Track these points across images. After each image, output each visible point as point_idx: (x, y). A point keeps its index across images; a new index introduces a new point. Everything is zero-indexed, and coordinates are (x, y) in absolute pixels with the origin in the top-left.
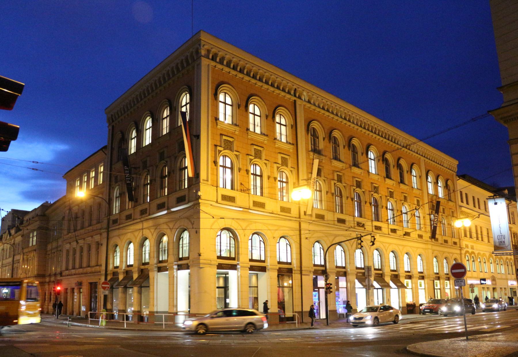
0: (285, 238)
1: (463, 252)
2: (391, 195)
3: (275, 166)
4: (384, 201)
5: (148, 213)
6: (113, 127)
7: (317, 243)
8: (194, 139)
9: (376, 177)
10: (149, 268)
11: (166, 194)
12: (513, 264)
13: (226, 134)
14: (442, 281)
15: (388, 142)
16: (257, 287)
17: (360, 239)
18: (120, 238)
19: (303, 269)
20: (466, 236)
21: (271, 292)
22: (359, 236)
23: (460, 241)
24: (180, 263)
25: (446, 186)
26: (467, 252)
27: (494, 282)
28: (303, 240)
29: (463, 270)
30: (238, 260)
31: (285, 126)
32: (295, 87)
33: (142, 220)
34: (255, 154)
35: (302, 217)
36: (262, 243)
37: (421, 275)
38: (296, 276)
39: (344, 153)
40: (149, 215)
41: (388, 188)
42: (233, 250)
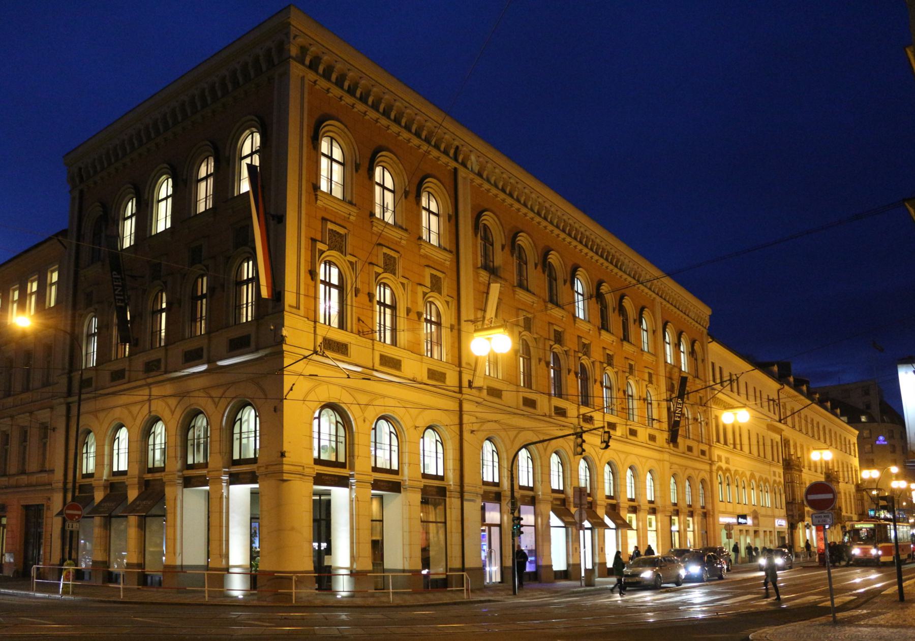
0: (434, 430)
1: (714, 468)
2: (610, 360)
3: (420, 290)
4: (598, 371)
5: (163, 369)
6: (81, 192)
7: (487, 442)
8: (272, 223)
9: (586, 327)
10: (165, 479)
11: (163, 344)
12: (782, 491)
13: (333, 220)
14: (682, 517)
15: (606, 264)
16: (382, 521)
17: (581, 437)
18: (97, 417)
19: (466, 488)
20: (718, 441)
21: (410, 532)
22: (579, 430)
23: (710, 449)
24: (235, 469)
25: (692, 353)
26: (720, 468)
27: (756, 522)
28: (466, 435)
29: (830, 496)
30: (352, 468)
31: (437, 215)
32: (456, 143)
33: (150, 380)
34: (386, 264)
35: (465, 390)
36: (393, 436)
37: (652, 506)
38: (453, 502)
39: (536, 278)
40: (166, 372)
41: (604, 348)
42: (341, 448)
